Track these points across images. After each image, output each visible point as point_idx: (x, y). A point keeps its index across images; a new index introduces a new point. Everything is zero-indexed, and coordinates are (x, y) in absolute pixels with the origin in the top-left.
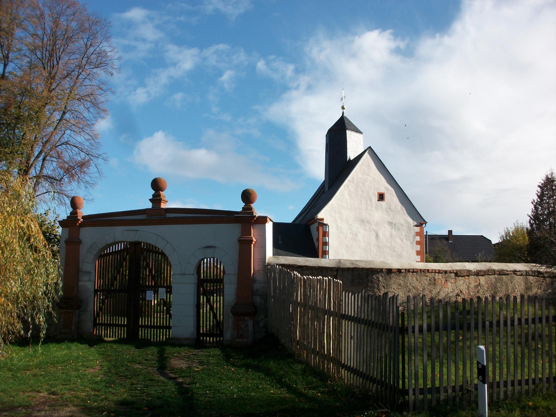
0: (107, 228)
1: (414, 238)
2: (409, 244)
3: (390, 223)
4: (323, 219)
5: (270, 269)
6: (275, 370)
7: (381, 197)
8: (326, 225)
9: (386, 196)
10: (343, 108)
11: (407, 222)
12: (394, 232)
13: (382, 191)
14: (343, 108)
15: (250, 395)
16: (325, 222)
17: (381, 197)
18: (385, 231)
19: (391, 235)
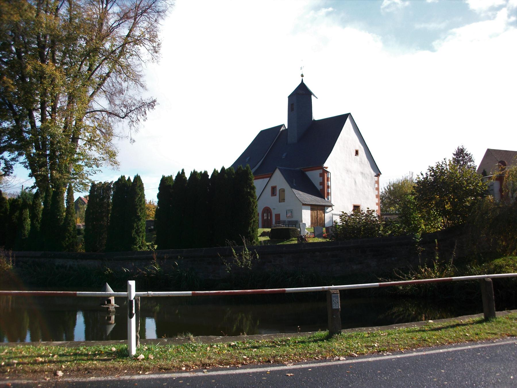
0: (284, 180)
1: (375, 185)
2: (372, 190)
3: (362, 173)
4: (327, 168)
5: (412, 349)
6: (85, 172)
7: (357, 153)
8: (328, 172)
9: (359, 152)
10: (302, 76)
11: (371, 173)
12: (364, 180)
13: (357, 148)
14: (302, 76)
15: (111, 350)
16: (328, 170)
17: (357, 153)
18: (359, 179)
19: (362, 181)
